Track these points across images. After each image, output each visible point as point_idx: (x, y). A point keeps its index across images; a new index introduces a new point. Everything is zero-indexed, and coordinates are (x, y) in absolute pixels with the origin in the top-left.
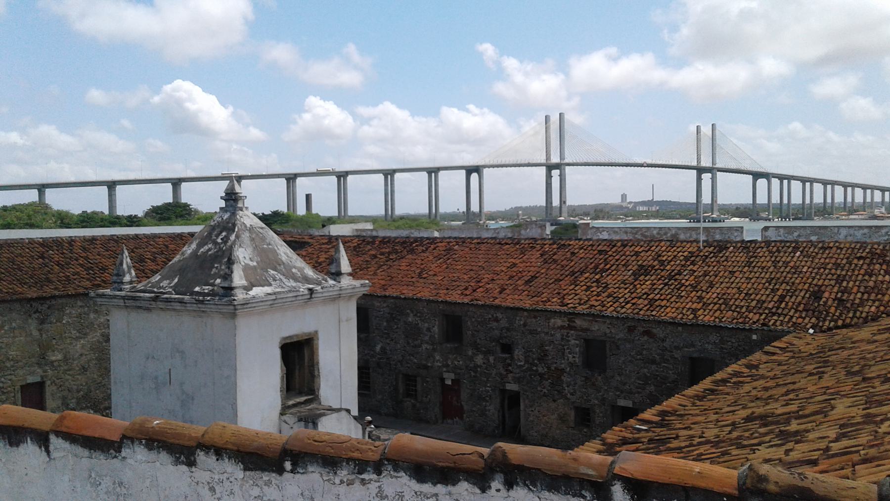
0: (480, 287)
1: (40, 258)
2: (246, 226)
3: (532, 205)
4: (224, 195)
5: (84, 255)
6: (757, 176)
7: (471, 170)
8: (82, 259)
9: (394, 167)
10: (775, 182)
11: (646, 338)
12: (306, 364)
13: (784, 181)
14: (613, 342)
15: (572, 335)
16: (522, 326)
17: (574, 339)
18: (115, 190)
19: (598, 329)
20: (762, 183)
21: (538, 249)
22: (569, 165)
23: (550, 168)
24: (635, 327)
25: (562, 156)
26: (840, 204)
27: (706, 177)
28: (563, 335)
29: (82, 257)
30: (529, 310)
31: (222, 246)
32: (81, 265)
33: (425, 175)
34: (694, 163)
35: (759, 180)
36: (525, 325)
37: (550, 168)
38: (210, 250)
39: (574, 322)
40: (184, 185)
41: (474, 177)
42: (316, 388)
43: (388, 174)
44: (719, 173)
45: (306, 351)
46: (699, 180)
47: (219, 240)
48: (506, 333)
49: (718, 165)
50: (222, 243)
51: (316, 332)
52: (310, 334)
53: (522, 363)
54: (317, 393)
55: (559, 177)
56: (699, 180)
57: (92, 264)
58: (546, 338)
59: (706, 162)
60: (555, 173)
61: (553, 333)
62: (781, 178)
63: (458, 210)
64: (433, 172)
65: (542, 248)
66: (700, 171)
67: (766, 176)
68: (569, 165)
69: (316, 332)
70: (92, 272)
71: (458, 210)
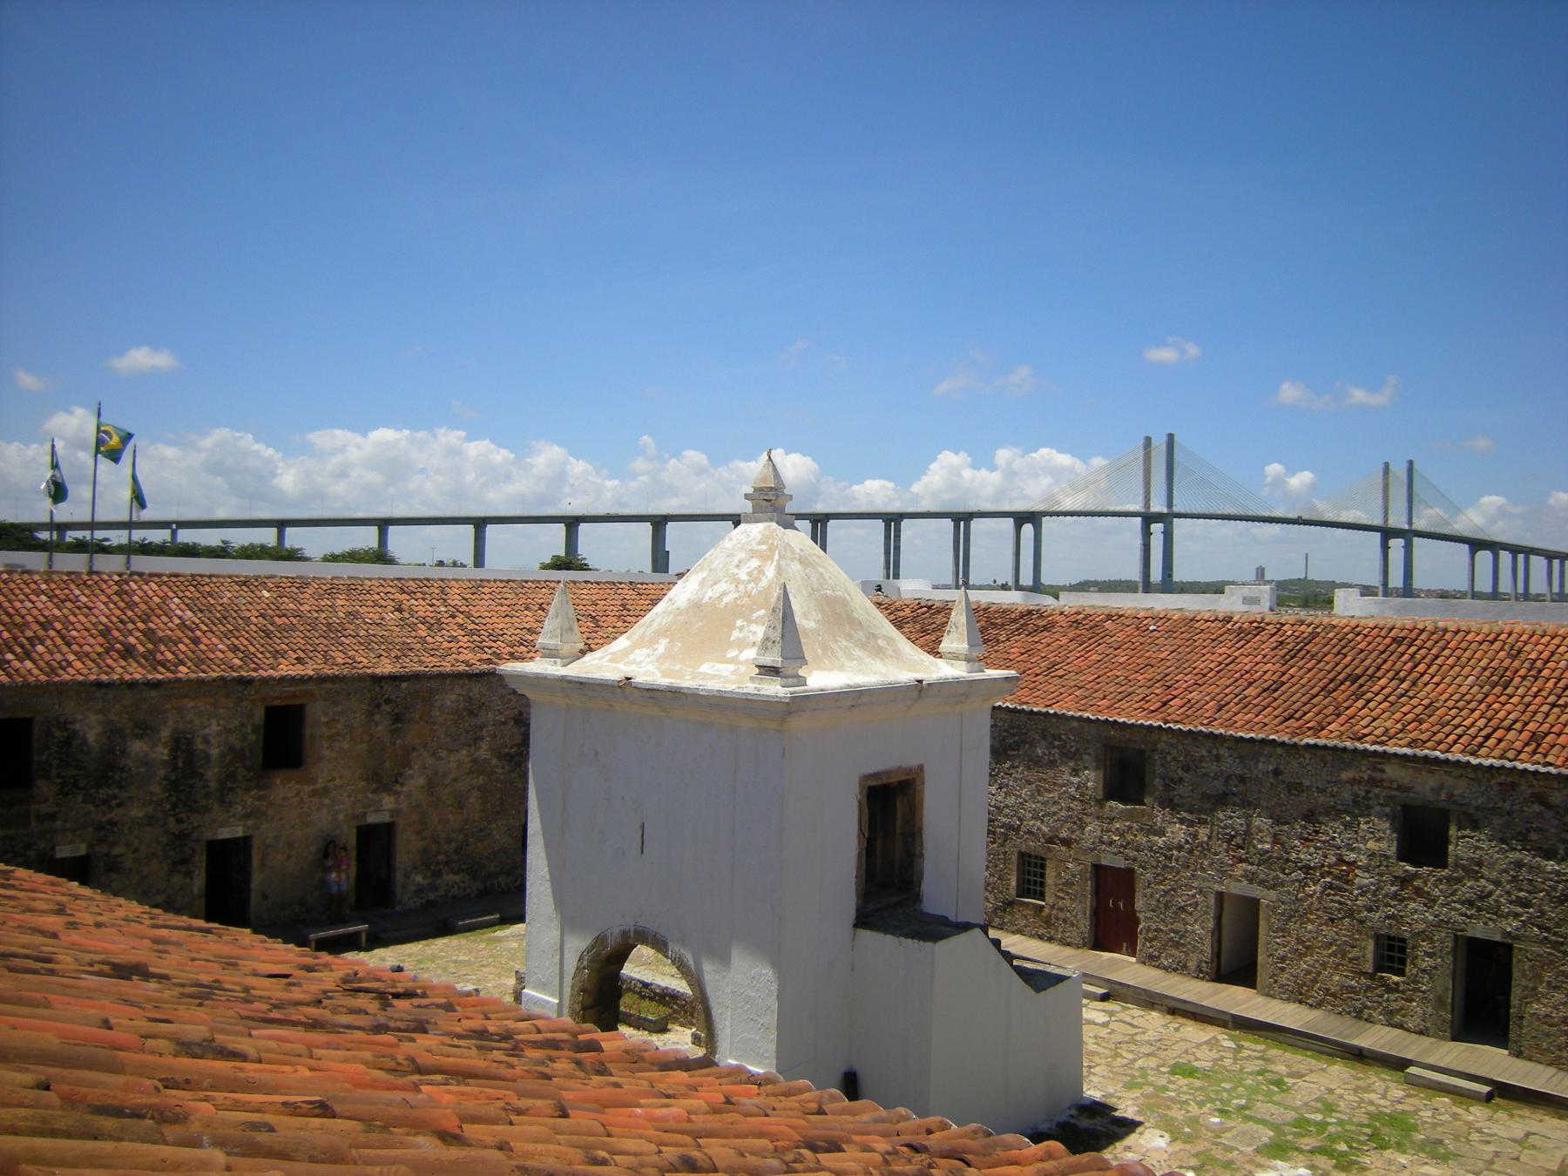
0: (1175, 697)
1: (397, 610)
2: (793, 552)
3: (1112, 579)
4: (750, 491)
5: (464, 608)
6: (1476, 545)
7: (1021, 518)
8: (462, 616)
9: (900, 510)
10: (1505, 557)
11: (1537, 808)
12: (898, 831)
14: (1465, 813)
15: (1377, 797)
16: (1271, 775)
17: (1380, 804)
18: (484, 532)
19: (1425, 785)
20: (1484, 557)
21: (1272, 632)
22: (1180, 516)
23: (1148, 519)
24: (1513, 786)
25: (1170, 504)
28: (1356, 795)
29: (462, 613)
30: (1288, 745)
31: (750, 587)
32: (460, 626)
33: (948, 524)
34: (1378, 522)
35: (1480, 552)
36: (1277, 772)
37: (1148, 519)
38: (724, 594)
39: (1383, 771)
40: (583, 527)
41: (1028, 529)
42: (915, 879)
43: (891, 520)
44: (1415, 539)
45: (898, 805)
47: (744, 577)
48: (1236, 786)
49: (1419, 524)
50: (749, 582)
51: (921, 767)
52: (910, 771)
53: (1267, 846)
54: (917, 889)
55: (1162, 535)
56: (1385, 548)
57: (477, 624)
58: (1321, 799)
59: (1398, 520)
60: (1157, 528)
61: (1335, 789)
62: (1515, 550)
63: (995, 582)
64: (962, 519)
65: (1279, 630)
66: (1387, 533)
67: (1493, 547)
68: (1180, 516)
69: (921, 767)
70: (478, 639)
71: (995, 582)
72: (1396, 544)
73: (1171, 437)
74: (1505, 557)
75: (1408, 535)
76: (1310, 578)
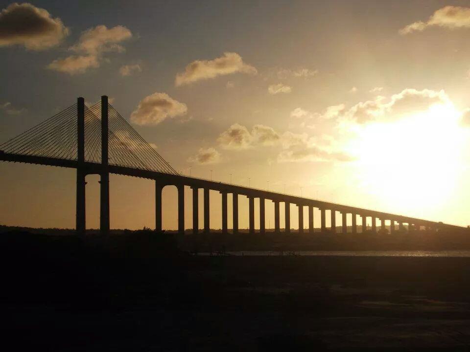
10: (188, 191)
20: (170, 192)
26: (188, 230)
27: (93, 181)
59: (93, 155)
72: (93, 181)
73: (105, 99)
74: (188, 191)
75: (104, 169)
76: (116, 223)
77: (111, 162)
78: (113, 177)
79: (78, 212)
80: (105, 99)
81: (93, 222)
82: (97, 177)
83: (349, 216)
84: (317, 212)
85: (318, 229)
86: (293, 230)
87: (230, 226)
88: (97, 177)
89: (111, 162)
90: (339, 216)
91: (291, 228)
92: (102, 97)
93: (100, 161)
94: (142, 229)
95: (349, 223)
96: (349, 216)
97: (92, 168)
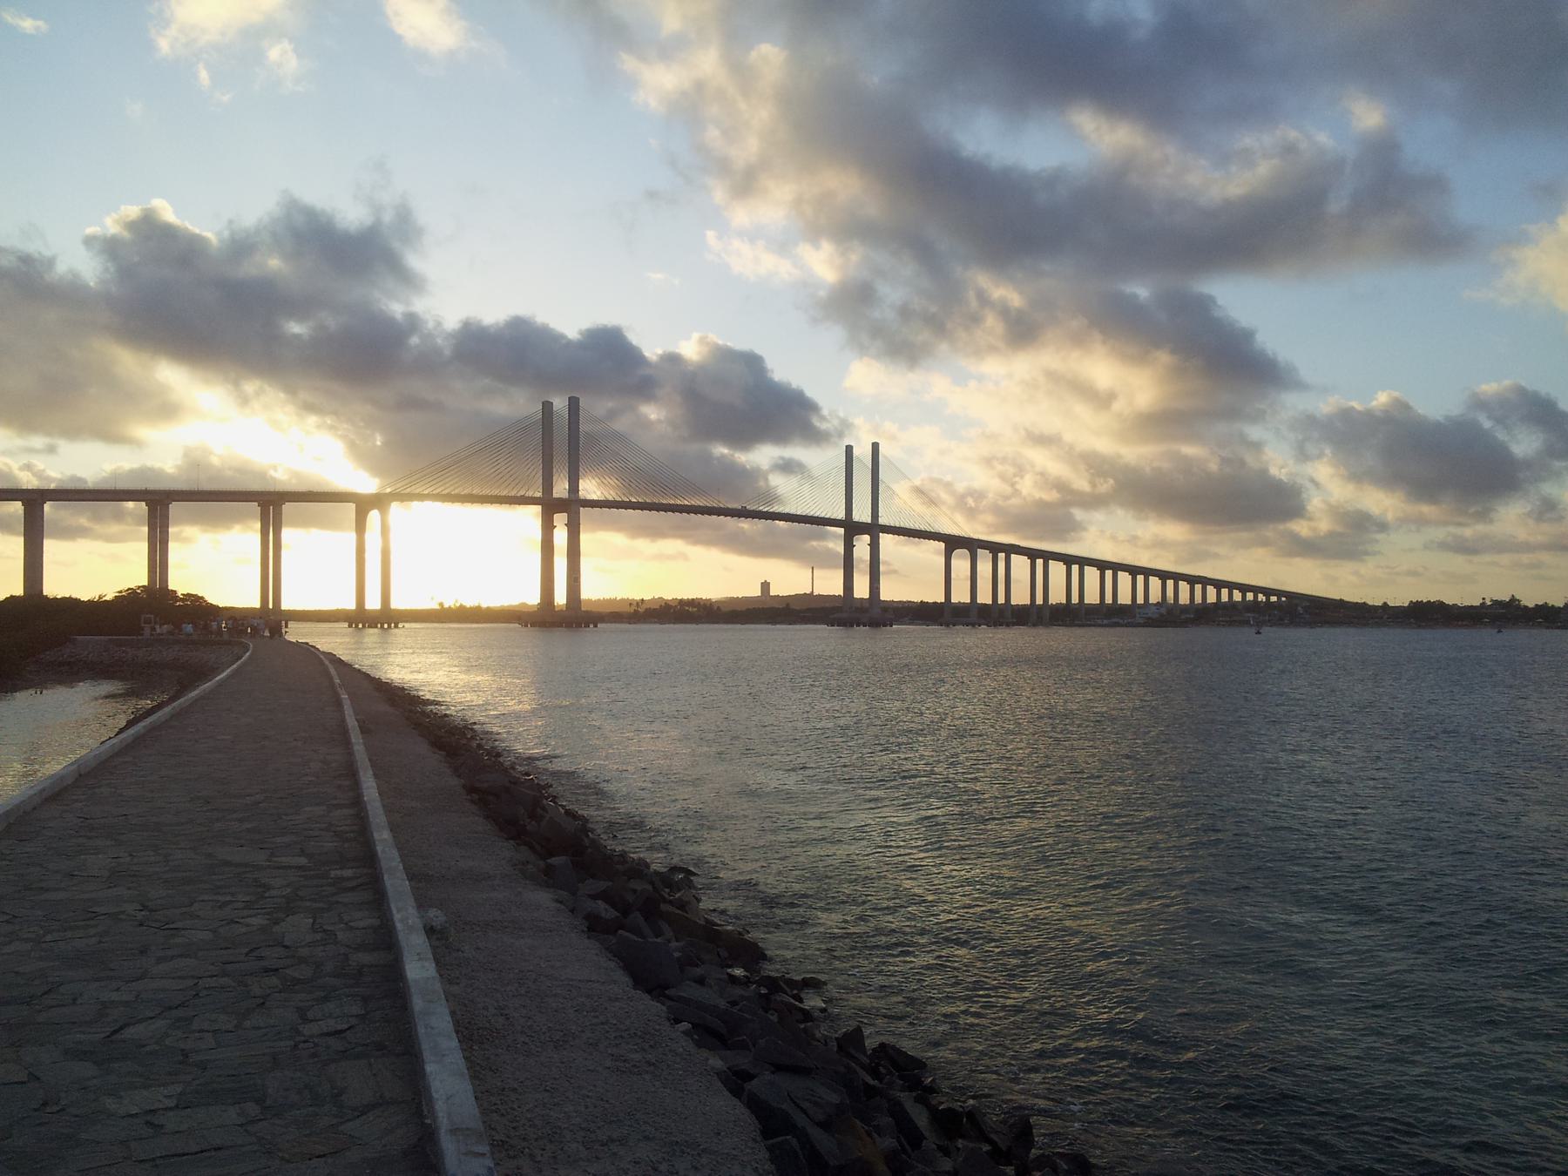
6: (953, 543)
13: (1223, 590)
20: (961, 563)
27: (862, 544)
46: (548, 528)
59: (862, 514)
66: (852, 528)
73: (875, 447)
75: (874, 529)
77: (882, 521)
78: (886, 540)
79: (1341, 604)
80: (875, 447)
81: (861, 590)
82: (867, 538)
83: (1225, 592)
84: (1184, 586)
85: (375, 611)
86: (559, 606)
87: (1001, 600)
88: (867, 538)
89: (882, 521)
90: (1211, 591)
91: (856, 595)
92: (873, 444)
93: (869, 520)
94: (1477, 603)
95: (1198, 599)
96: (1225, 592)
97: (861, 528)
